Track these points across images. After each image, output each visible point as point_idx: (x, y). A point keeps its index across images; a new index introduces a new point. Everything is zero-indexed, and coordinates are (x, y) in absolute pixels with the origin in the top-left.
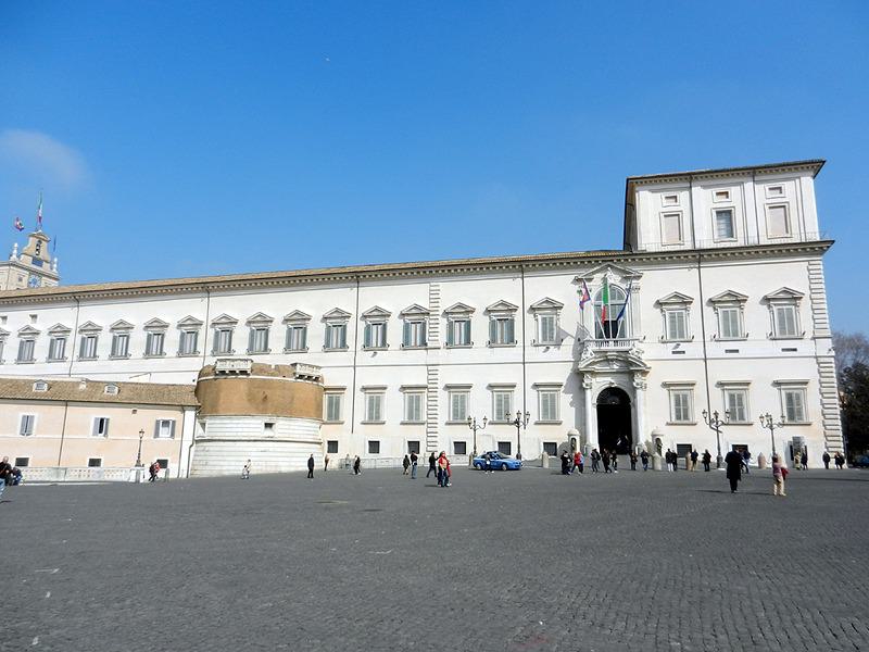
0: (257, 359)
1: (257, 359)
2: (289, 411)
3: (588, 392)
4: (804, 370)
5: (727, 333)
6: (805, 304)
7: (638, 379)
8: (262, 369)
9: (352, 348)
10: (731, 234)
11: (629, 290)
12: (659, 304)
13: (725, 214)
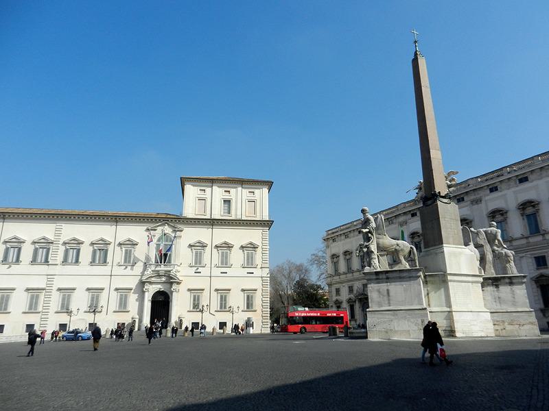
3: (146, 294)
4: (255, 283)
6: (259, 250)
7: (174, 286)
9: (110, 264)
12: (190, 246)
13: (227, 202)
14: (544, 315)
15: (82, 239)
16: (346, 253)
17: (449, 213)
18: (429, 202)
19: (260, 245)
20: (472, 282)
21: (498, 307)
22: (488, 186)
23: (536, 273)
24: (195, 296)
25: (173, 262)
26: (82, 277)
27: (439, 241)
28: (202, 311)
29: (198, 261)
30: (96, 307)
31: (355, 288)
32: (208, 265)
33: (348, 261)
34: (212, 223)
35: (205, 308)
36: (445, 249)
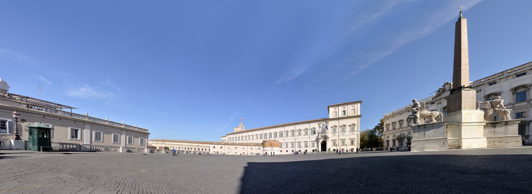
0: (270, 139)
1: (270, 139)
2: (275, 146)
4: (355, 137)
6: (356, 126)
8: (270, 140)
12: (332, 127)
13: (344, 111)
19: (357, 124)
20: (478, 126)
21: (490, 136)
22: (489, 82)
23: (392, 139)
24: (334, 142)
26: (303, 138)
27: (459, 108)
28: (337, 146)
29: (334, 131)
30: (307, 146)
34: (339, 119)
35: (338, 145)
36: (462, 112)
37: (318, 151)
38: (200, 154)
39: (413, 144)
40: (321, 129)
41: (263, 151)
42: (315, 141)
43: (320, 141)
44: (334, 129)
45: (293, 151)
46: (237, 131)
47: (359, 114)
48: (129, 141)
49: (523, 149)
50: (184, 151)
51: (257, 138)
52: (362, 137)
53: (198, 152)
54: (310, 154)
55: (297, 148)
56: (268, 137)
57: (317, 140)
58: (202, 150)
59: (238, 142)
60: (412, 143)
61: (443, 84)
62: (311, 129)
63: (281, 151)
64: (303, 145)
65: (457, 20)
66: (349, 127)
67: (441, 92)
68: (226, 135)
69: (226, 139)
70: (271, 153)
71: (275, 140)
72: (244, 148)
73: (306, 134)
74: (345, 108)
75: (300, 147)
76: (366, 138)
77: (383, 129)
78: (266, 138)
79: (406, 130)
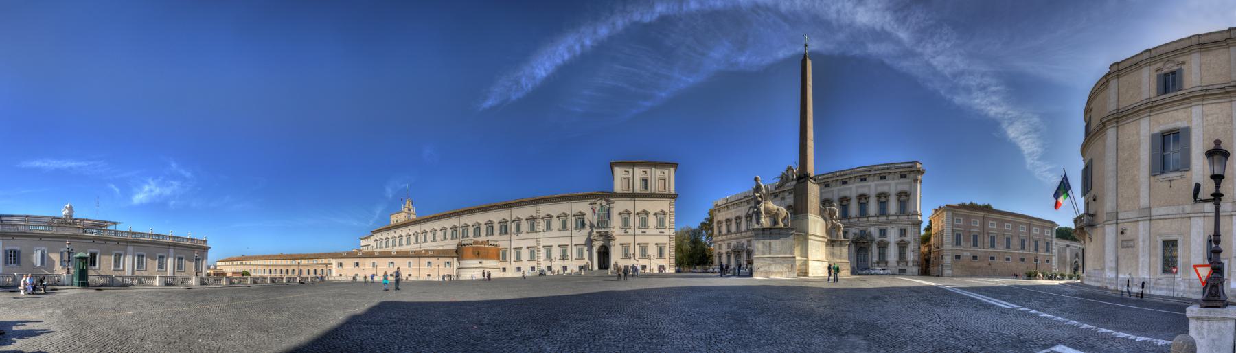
0: (476, 239)
1: (476, 239)
2: (487, 257)
3: (594, 248)
4: (665, 240)
5: (642, 226)
6: (668, 216)
7: (612, 242)
8: (476, 243)
10: (646, 188)
11: (609, 208)
12: (620, 214)
13: (645, 180)
14: (898, 265)
15: (552, 214)
16: (727, 220)
17: (814, 190)
18: (802, 181)
25: (609, 226)
26: (554, 239)
28: (630, 258)
29: (626, 224)
31: (732, 245)
32: (633, 227)
33: (738, 225)
34: (634, 196)
35: (632, 256)
36: (809, 217)
37: (592, 269)
38: (302, 283)
39: (756, 264)
40: (596, 217)
41: (458, 268)
42: (585, 245)
43: (595, 245)
44: (625, 219)
45: (533, 269)
46: (399, 221)
47: (673, 191)
48: (178, 265)
49: (854, 280)
50: (266, 278)
51: (445, 238)
52: (680, 243)
53: (298, 278)
54: (573, 276)
55: (542, 262)
56: (471, 234)
57: (590, 242)
58: (309, 274)
59: (398, 248)
60: (755, 261)
61: (786, 168)
62: (574, 216)
63: (504, 270)
64: (556, 253)
65: (802, 58)
66: (655, 216)
67: (785, 179)
68: (371, 234)
69: (371, 244)
70: (484, 276)
71: (488, 241)
72: (410, 263)
73: (563, 228)
74: (646, 172)
75: (549, 258)
76: (687, 246)
77: (712, 229)
78: (468, 236)
79: (745, 237)
